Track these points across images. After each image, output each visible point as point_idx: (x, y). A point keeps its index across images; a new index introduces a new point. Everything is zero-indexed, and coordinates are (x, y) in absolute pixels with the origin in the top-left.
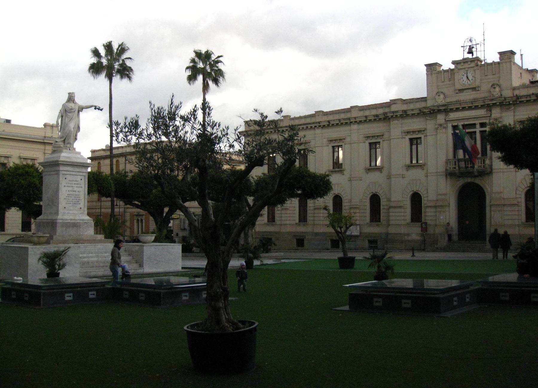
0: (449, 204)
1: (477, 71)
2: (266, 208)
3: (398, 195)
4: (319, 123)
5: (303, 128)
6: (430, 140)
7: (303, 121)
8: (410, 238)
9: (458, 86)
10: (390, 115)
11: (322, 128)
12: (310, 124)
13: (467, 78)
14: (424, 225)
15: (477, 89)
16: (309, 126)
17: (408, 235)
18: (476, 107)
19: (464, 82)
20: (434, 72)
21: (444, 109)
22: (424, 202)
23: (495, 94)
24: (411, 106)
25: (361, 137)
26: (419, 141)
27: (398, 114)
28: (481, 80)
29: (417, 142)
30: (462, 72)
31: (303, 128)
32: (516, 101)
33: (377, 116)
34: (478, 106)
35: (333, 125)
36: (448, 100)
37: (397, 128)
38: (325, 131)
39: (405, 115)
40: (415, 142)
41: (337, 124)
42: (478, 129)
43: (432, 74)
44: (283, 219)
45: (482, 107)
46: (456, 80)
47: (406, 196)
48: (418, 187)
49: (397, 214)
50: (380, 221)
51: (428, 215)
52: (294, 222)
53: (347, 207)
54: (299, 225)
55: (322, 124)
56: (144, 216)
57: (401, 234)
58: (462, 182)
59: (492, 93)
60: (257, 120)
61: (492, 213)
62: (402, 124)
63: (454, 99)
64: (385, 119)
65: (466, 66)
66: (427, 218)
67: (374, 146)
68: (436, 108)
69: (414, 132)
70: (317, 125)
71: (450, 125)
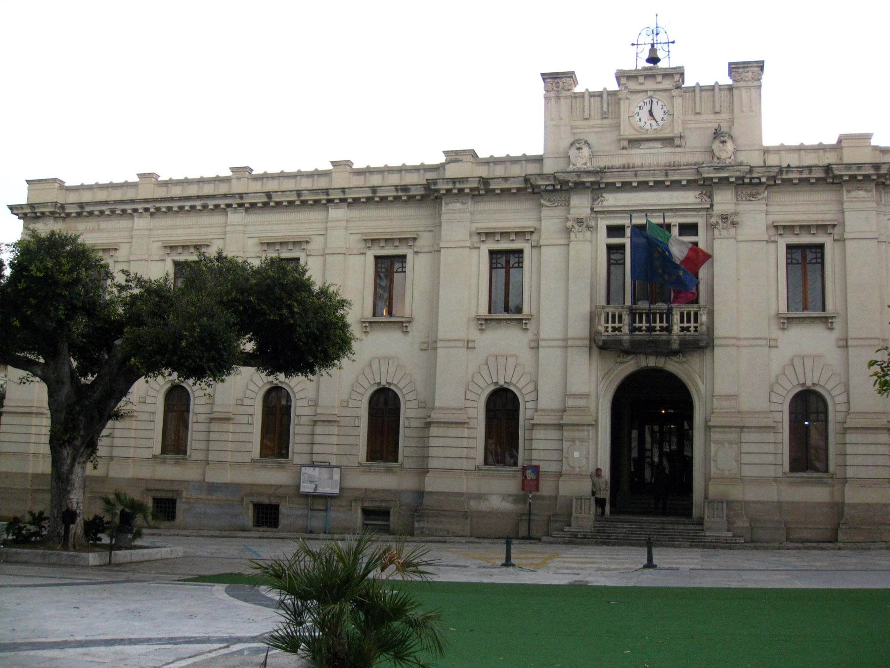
0: (597, 421)
1: (678, 102)
3: (456, 392)
4: (241, 196)
6: (551, 256)
7: (101, 196)
8: (483, 506)
9: (627, 132)
10: (443, 186)
11: (247, 209)
12: (214, 197)
13: (651, 113)
14: (530, 474)
15: (677, 142)
16: (211, 203)
17: (480, 497)
18: (676, 185)
19: (642, 124)
20: (564, 93)
21: (592, 183)
22: (525, 413)
23: (724, 156)
24: (499, 171)
25: (354, 243)
26: (513, 260)
28: (684, 122)
29: (508, 262)
30: (638, 100)
31: (170, 209)
32: (774, 178)
33: (405, 188)
34: (679, 182)
36: (601, 163)
37: (459, 222)
38: (254, 218)
39: (484, 190)
40: (503, 261)
41: (291, 203)
43: (558, 98)
45: (691, 184)
46: (624, 116)
47: (475, 397)
48: (510, 372)
49: (449, 442)
50: (396, 460)
51: (537, 446)
52: (147, 454)
53: (304, 420)
54: (164, 461)
55: (247, 201)
57: (461, 494)
58: (629, 366)
59: (717, 153)
61: (713, 447)
62: (472, 213)
63: (618, 161)
64: (423, 198)
65: (649, 85)
66: (535, 455)
68: (573, 178)
69: (504, 234)
70: (234, 202)
71: (602, 225)
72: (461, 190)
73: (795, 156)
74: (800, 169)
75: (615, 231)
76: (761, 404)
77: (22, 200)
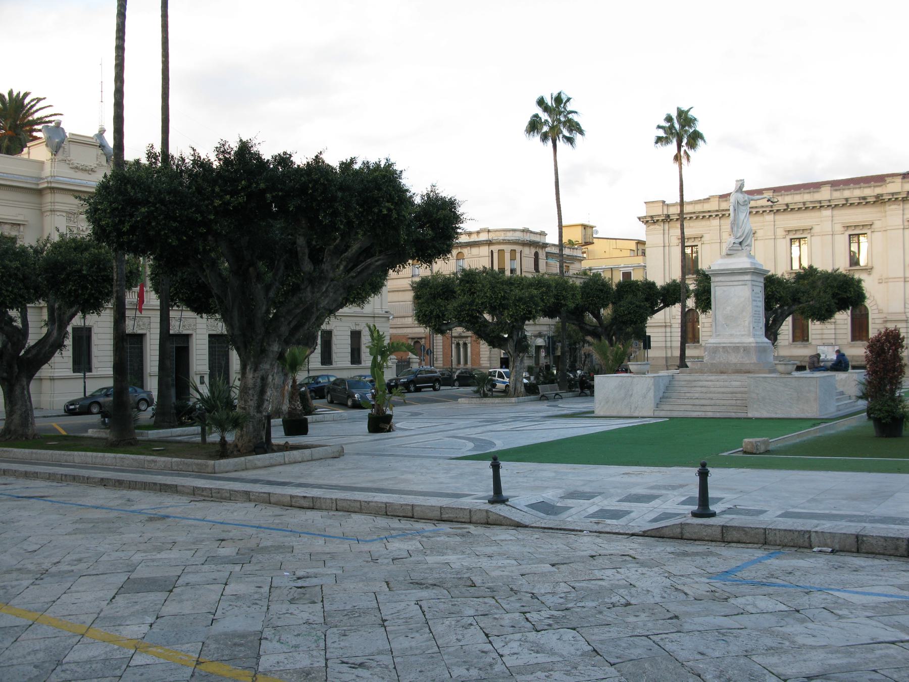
2: (789, 319)
5: (691, 218)
35: (792, 209)
44: (833, 332)
56: (469, 339)
67: (856, 239)
72: (896, 199)
73: (502, 233)
77: (643, 213)
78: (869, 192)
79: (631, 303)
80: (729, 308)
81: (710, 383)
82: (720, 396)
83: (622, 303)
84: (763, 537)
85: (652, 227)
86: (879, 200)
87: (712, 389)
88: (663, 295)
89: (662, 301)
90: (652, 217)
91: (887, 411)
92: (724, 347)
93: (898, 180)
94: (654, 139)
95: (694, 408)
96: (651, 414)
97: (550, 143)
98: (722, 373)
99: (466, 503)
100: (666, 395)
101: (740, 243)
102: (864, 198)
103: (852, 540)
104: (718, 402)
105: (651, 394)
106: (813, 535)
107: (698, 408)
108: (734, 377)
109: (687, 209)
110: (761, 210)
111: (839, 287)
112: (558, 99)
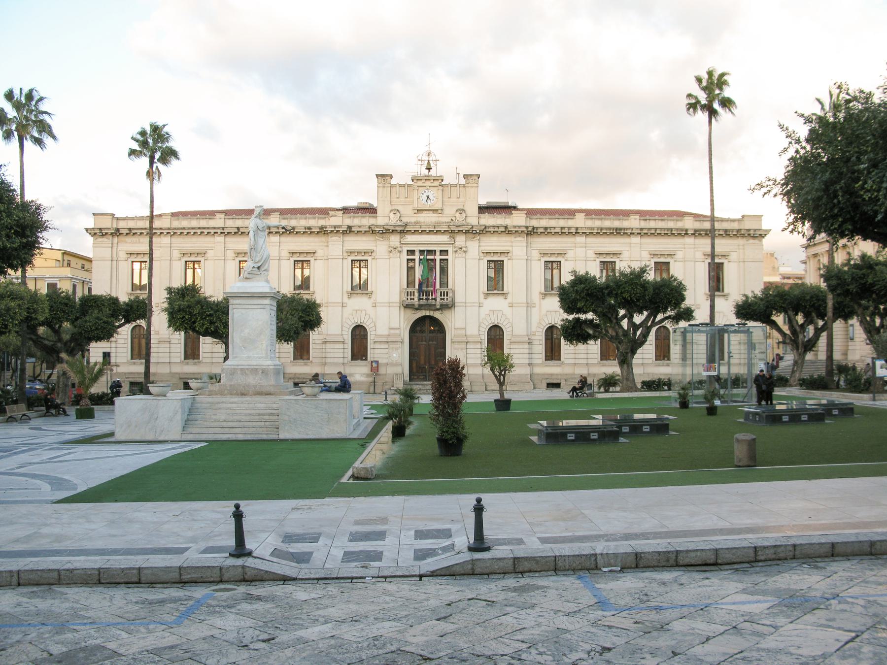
14: (374, 365)
27: (341, 229)
38: (230, 240)
42: (438, 257)
50: (309, 359)
51: (374, 351)
55: (226, 231)
60: (869, 254)
63: (413, 220)
65: (428, 183)
67: (300, 265)
70: (219, 231)
71: (405, 249)
74: (494, 227)
75: (412, 252)
76: (476, 332)
78: (315, 223)
79: (97, 318)
80: (247, 331)
81: (234, 405)
82: (248, 417)
83: (87, 318)
84: (553, 564)
85: (100, 240)
86: (323, 231)
87: (237, 411)
88: (127, 311)
89: (124, 317)
90: (101, 229)
91: (453, 433)
92: (242, 369)
93: (340, 214)
94: (127, 151)
95: (222, 431)
96: (178, 438)
97: (15, 141)
98: (242, 394)
99: (194, 557)
100: (191, 417)
101: (258, 268)
102: (309, 228)
103: (633, 557)
104: (246, 424)
105: (179, 417)
106: (599, 557)
107: (227, 430)
108: (258, 398)
109: (157, 224)
110: (212, 231)
111: (303, 311)
112: (29, 96)
